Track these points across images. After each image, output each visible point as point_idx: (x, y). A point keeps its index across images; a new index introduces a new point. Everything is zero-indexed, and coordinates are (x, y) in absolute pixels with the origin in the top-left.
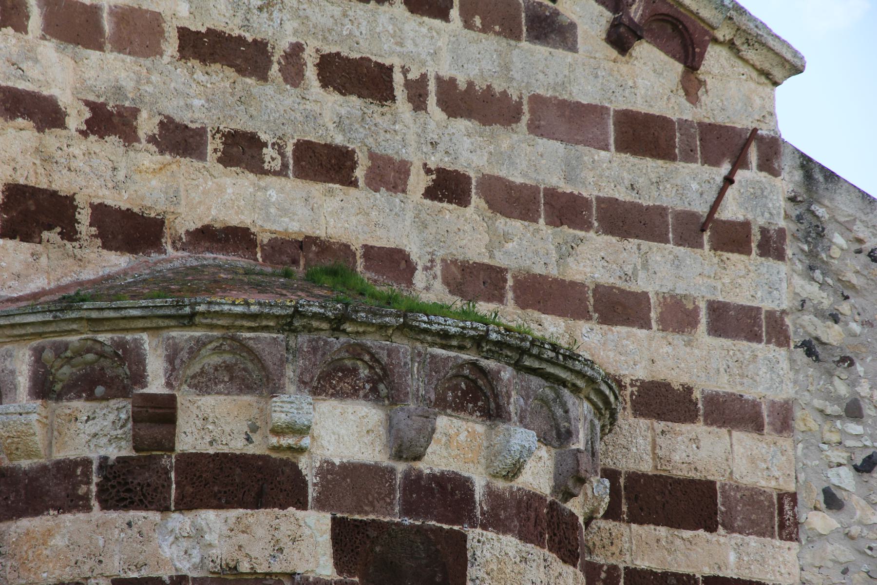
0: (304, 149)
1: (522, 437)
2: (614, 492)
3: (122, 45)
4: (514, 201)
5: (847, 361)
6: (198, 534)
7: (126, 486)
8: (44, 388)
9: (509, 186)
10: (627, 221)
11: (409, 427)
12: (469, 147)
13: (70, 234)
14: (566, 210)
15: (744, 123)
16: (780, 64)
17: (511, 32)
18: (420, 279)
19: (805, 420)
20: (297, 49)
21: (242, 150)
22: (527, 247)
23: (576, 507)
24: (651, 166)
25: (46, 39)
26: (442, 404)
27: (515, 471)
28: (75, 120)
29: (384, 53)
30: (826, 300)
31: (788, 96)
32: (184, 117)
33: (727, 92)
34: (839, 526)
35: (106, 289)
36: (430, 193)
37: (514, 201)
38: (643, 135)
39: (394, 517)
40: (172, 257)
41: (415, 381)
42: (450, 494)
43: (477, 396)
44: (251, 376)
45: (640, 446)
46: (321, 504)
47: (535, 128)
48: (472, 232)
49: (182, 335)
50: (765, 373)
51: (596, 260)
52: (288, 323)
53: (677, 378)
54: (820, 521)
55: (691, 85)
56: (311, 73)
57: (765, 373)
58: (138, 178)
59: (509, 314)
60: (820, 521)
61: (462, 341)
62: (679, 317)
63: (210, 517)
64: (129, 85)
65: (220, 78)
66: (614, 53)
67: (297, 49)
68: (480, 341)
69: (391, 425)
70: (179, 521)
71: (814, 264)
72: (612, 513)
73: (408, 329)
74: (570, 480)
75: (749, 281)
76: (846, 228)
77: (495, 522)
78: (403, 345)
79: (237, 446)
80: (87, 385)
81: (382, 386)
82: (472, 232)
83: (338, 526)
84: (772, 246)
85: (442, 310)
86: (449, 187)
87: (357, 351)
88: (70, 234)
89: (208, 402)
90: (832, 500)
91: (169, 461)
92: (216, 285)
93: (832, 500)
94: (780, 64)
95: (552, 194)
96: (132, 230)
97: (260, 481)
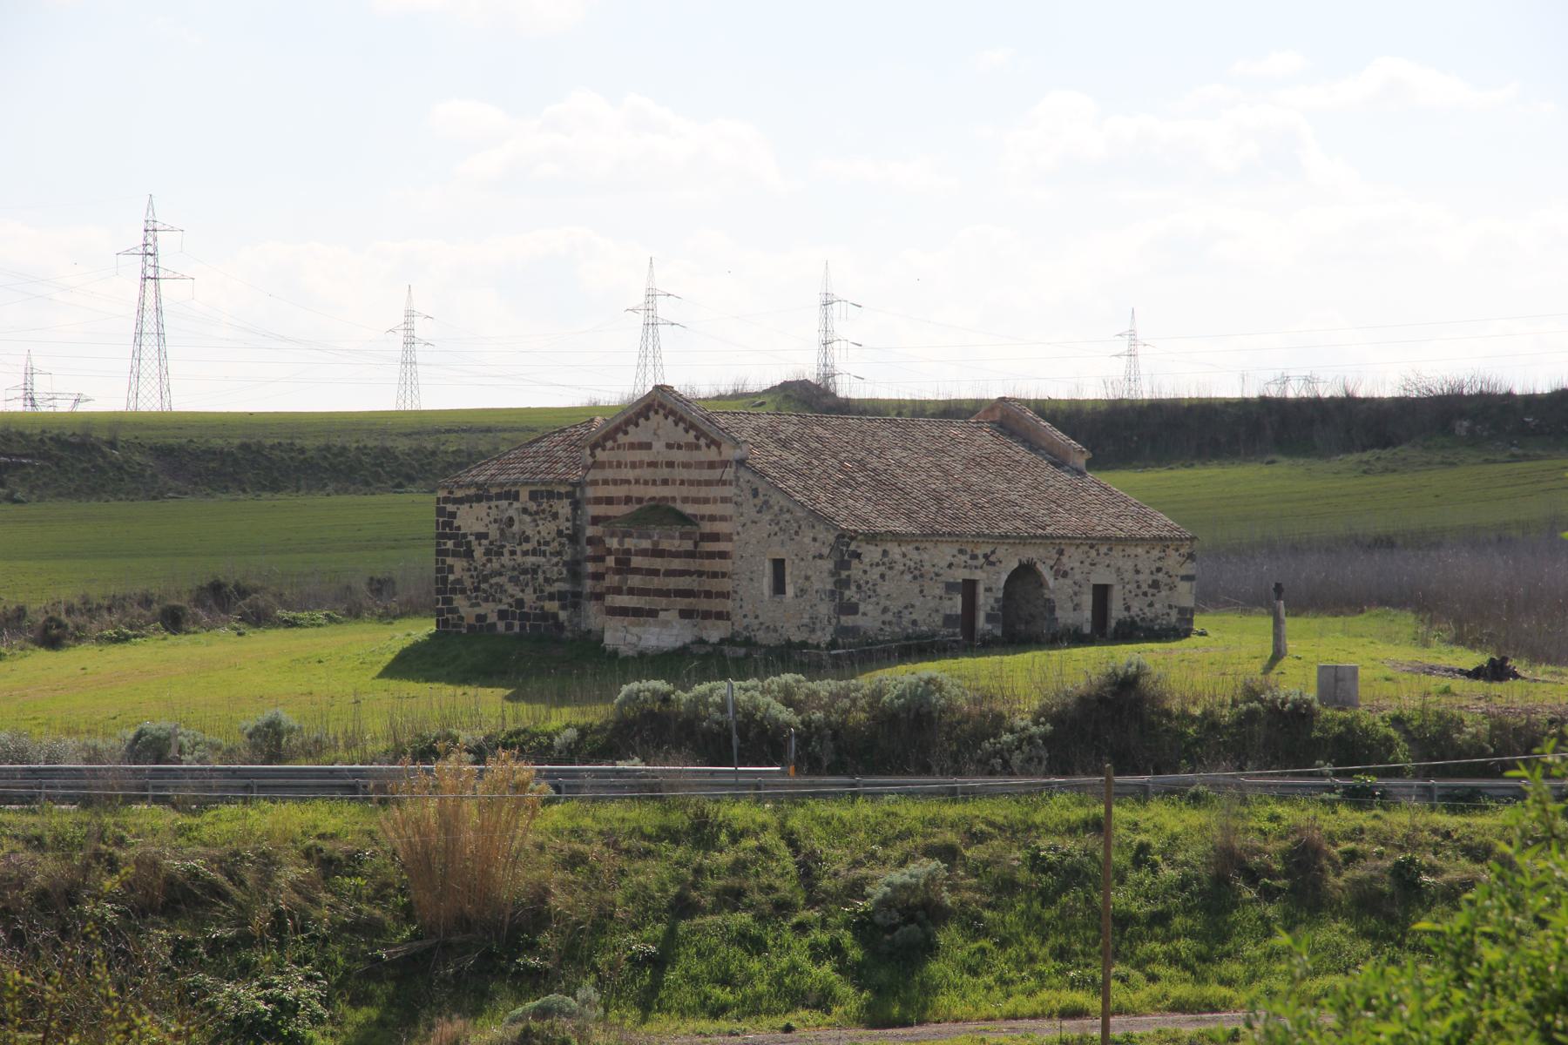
4: (692, 483)
14: (699, 483)
25: (203, 606)
37: (692, 483)
38: (712, 465)
50: (728, 509)
57: (728, 509)
58: (637, 491)
96: (640, 500)
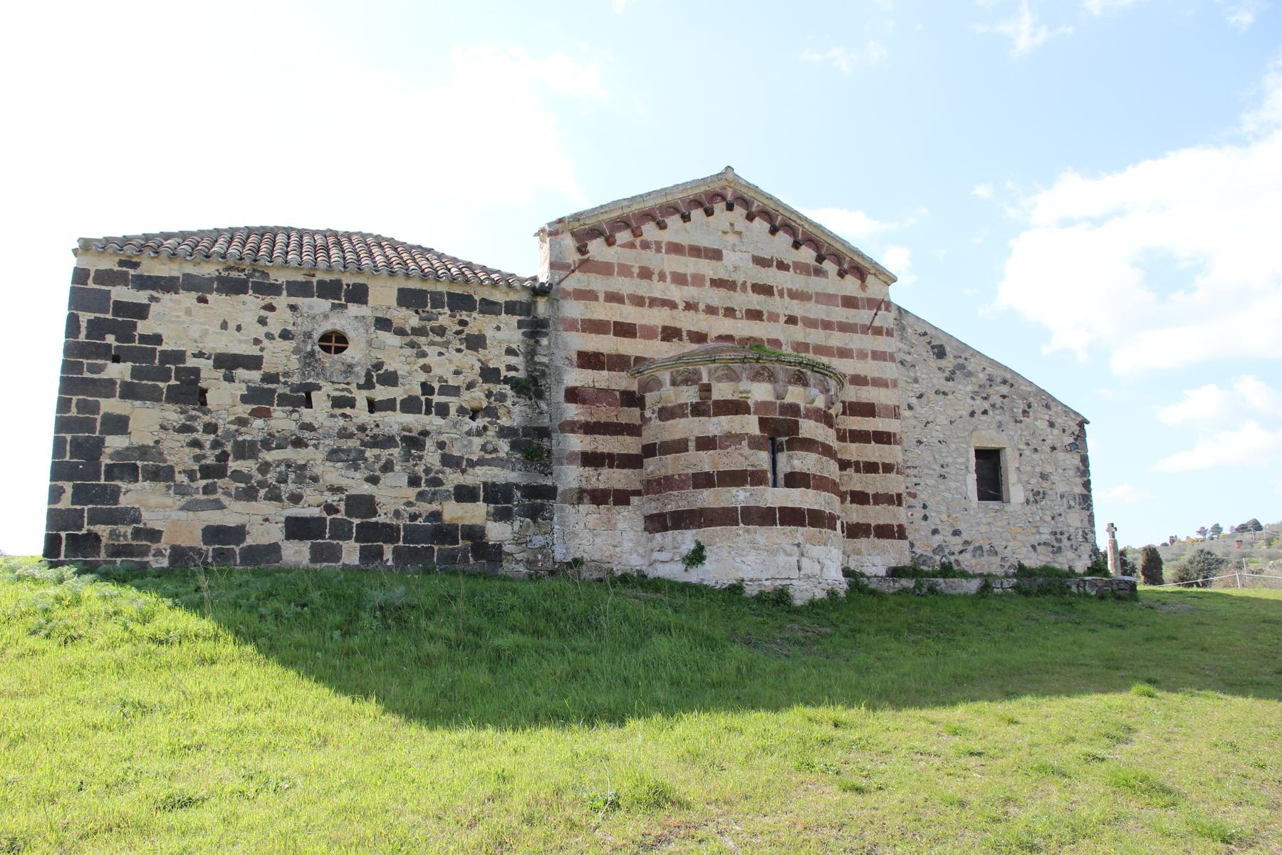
1: (814, 391)
2: (844, 407)
4: (811, 323)
5: (913, 366)
6: (719, 423)
7: (698, 410)
8: (674, 383)
10: (845, 328)
11: (780, 389)
12: (797, 308)
13: (681, 339)
14: (827, 325)
15: (880, 297)
16: (890, 279)
17: (808, 274)
18: (784, 347)
19: (901, 384)
20: (745, 282)
21: (730, 312)
22: (816, 337)
23: (832, 412)
24: (852, 311)
26: (790, 382)
27: (813, 401)
28: (681, 306)
30: (906, 348)
31: (892, 289)
32: (712, 304)
33: (874, 288)
34: (500, 572)
35: (691, 354)
37: (811, 323)
38: (850, 302)
39: (777, 416)
40: (710, 344)
41: (781, 376)
42: (793, 409)
43: (800, 380)
44: (733, 377)
45: (852, 394)
46: (755, 413)
47: (817, 302)
48: (799, 333)
49: (712, 366)
50: (888, 370)
51: (837, 339)
52: (743, 361)
54: (906, 413)
55: (863, 287)
56: (749, 289)
57: (888, 370)
58: (699, 322)
59: (811, 356)
60: (906, 413)
61: (795, 364)
62: (862, 355)
63: (722, 418)
64: (696, 295)
65: (722, 292)
66: (993, 505)
67: (745, 282)
68: (800, 363)
69: (775, 390)
70: (714, 419)
71: (902, 338)
72: (844, 413)
73: (778, 361)
74: (830, 404)
75: (882, 343)
76: (912, 327)
77: (807, 416)
78: (777, 366)
79: (729, 397)
80: (686, 382)
81: (772, 378)
82: (799, 333)
83: (760, 419)
84: (889, 333)
85: (789, 355)
86: (792, 320)
87: (764, 368)
88: (681, 339)
89: (721, 385)
90: (910, 407)
91: (710, 402)
92: (723, 351)
93: (910, 407)
94: (890, 279)
95: (823, 321)
96: (699, 337)
97: (736, 407)
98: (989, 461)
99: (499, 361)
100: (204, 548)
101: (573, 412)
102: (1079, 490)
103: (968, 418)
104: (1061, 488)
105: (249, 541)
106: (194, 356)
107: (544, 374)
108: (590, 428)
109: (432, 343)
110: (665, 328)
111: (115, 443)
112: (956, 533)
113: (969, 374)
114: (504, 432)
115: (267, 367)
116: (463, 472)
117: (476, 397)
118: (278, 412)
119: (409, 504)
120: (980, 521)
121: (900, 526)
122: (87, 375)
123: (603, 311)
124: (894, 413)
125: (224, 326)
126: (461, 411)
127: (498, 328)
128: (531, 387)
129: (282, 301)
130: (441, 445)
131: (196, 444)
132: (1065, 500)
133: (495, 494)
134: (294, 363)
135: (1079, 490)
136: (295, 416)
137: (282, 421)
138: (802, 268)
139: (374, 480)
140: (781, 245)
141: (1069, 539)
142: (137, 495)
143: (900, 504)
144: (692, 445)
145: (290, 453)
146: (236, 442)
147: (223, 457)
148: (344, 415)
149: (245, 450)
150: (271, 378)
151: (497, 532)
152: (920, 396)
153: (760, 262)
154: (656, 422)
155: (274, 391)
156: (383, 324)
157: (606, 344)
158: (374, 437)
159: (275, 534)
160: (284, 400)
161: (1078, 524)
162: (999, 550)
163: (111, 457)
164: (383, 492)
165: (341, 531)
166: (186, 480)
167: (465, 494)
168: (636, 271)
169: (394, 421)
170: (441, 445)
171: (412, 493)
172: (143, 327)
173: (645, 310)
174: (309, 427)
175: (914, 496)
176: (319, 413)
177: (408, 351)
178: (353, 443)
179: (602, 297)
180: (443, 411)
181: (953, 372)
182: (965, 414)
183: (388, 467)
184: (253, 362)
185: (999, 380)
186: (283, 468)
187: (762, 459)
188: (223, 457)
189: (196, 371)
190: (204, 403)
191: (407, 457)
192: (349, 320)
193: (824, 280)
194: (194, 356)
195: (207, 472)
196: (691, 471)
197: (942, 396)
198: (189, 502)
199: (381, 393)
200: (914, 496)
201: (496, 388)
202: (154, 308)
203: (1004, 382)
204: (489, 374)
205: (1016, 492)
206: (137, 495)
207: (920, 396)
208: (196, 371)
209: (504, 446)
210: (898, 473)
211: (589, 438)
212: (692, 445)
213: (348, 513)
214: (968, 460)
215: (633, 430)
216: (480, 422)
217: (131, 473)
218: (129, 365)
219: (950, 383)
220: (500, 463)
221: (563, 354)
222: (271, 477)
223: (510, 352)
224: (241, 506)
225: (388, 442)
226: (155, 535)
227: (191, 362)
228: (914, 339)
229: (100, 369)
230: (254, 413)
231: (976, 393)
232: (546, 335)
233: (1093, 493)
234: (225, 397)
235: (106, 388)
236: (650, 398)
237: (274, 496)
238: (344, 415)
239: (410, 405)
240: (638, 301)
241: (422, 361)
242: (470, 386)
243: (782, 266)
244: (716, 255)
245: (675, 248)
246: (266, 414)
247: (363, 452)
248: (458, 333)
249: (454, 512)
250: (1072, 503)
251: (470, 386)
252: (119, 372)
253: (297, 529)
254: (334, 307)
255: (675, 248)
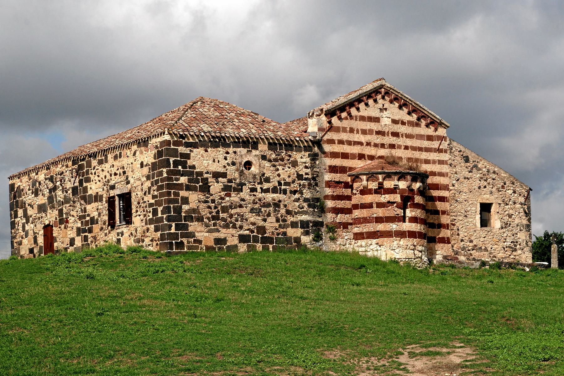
0: (390, 145)
3: (369, 134)
4: (414, 149)
7: (377, 192)
9: (413, 147)
10: (428, 150)
13: (365, 159)
14: (420, 149)
21: (383, 146)
22: (417, 155)
28: (365, 145)
29: (399, 131)
30: (453, 158)
36: (404, 149)
37: (414, 149)
38: (430, 138)
50: (445, 169)
51: (424, 156)
53: (434, 171)
57: (445, 169)
62: (434, 162)
63: (386, 195)
84: (446, 151)
86: (406, 148)
88: (365, 159)
95: (419, 147)
97: (393, 191)
98: (486, 208)
99: (303, 171)
100: (215, 246)
101: (328, 191)
102: (525, 222)
103: (478, 190)
104: (517, 221)
105: (228, 244)
106: (206, 173)
107: (318, 176)
108: (334, 198)
109: (280, 165)
110: (359, 154)
111: (185, 207)
112: (471, 241)
113: (480, 169)
114: (306, 200)
115: (228, 177)
116: (293, 217)
117: (295, 186)
118: (233, 194)
119: (277, 229)
120: (479, 236)
121: (448, 238)
122: (175, 182)
123: (337, 148)
124: (446, 188)
125: (214, 161)
126: (291, 192)
127: (302, 158)
128: (314, 182)
129: (231, 150)
130: (285, 206)
131: (209, 207)
132: (519, 227)
133: (304, 225)
134: (237, 175)
135: (525, 222)
136: (239, 196)
137: (235, 198)
138: (411, 124)
139: (265, 220)
140: (403, 114)
141: (520, 245)
142: (194, 226)
143: (448, 229)
144: (375, 205)
145: (238, 210)
146: (222, 206)
147: (218, 212)
148: (254, 195)
149: (225, 209)
150: (230, 181)
151: (305, 239)
152: (458, 180)
153: (395, 122)
154: (358, 196)
155: (231, 186)
156: (264, 157)
157: (338, 162)
158: (264, 203)
159: (235, 241)
160: (235, 190)
161: (524, 238)
162: (489, 249)
163: (185, 213)
164: (268, 225)
165: (256, 240)
166: (207, 221)
167: (294, 225)
168: (348, 129)
169: (270, 197)
170: (285, 206)
171: (277, 225)
172: (190, 163)
173: (352, 147)
174: (243, 200)
175: (454, 225)
176: (245, 193)
177: (272, 168)
178: (257, 206)
179: (336, 142)
180: (285, 192)
181: (472, 169)
182: (476, 188)
183: (269, 215)
184: (224, 175)
185: (492, 172)
186: (236, 216)
187: (400, 212)
188: (218, 212)
189: (207, 179)
190: (209, 191)
191: (275, 211)
192: (253, 156)
193: (419, 128)
194: (206, 173)
195: (214, 218)
196: (375, 215)
197: (467, 180)
198: (209, 230)
199: (266, 186)
200: (454, 225)
201: (302, 182)
202: (192, 154)
203: (494, 172)
204: (300, 177)
205: (496, 223)
206: (194, 226)
207: (458, 180)
208: (207, 179)
209: (305, 205)
210: (447, 215)
211: (334, 202)
212: (375, 205)
213: (258, 233)
214: (476, 208)
215: (349, 198)
216: (297, 196)
217: (191, 219)
218: (187, 177)
219: (470, 174)
220: (305, 213)
221: (324, 167)
222: (233, 220)
223: (306, 167)
224: (224, 231)
225: (268, 205)
226: (200, 242)
227: (205, 176)
228: (457, 153)
229: (178, 180)
230: (226, 195)
231: (482, 178)
232: (318, 159)
233: (532, 224)
234: (216, 187)
235: (180, 187)
236: (356, 185)
237: (234, 227)
238: (254, 195)
239: (275, 190)
240: (349, 143)
241: (277, 173)
242: (293, 182)
243: (403, 123)
244: (377, 120)
245: (363, 118)
246: (229, 195)
247: (261, 209)
248: (288, 160)
249: (292, 232)
250: (522, 228)
251: (293, 182)
252: (183, 180)
253: (243, 239)
254: (248, 151)
255: (363, 118)
